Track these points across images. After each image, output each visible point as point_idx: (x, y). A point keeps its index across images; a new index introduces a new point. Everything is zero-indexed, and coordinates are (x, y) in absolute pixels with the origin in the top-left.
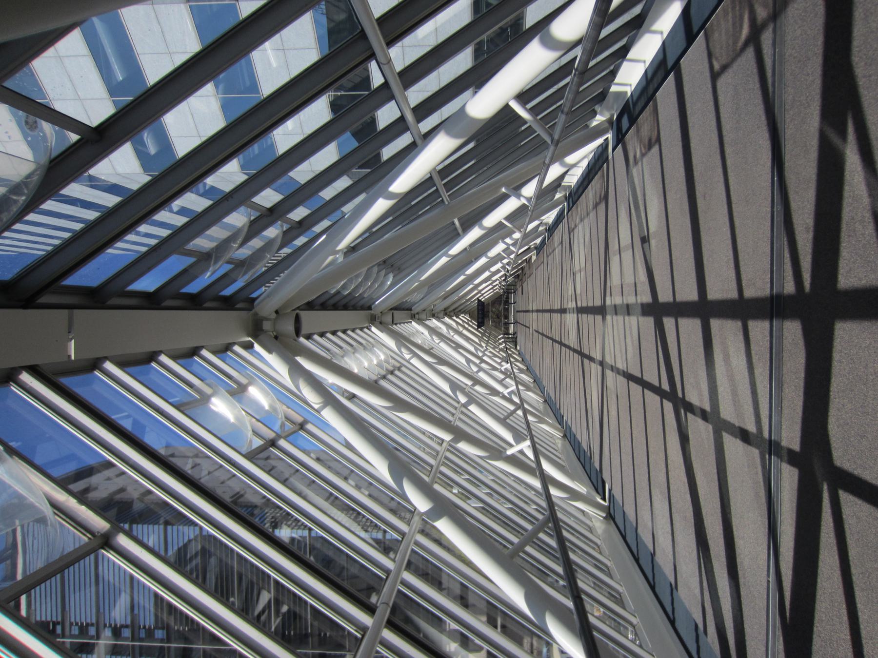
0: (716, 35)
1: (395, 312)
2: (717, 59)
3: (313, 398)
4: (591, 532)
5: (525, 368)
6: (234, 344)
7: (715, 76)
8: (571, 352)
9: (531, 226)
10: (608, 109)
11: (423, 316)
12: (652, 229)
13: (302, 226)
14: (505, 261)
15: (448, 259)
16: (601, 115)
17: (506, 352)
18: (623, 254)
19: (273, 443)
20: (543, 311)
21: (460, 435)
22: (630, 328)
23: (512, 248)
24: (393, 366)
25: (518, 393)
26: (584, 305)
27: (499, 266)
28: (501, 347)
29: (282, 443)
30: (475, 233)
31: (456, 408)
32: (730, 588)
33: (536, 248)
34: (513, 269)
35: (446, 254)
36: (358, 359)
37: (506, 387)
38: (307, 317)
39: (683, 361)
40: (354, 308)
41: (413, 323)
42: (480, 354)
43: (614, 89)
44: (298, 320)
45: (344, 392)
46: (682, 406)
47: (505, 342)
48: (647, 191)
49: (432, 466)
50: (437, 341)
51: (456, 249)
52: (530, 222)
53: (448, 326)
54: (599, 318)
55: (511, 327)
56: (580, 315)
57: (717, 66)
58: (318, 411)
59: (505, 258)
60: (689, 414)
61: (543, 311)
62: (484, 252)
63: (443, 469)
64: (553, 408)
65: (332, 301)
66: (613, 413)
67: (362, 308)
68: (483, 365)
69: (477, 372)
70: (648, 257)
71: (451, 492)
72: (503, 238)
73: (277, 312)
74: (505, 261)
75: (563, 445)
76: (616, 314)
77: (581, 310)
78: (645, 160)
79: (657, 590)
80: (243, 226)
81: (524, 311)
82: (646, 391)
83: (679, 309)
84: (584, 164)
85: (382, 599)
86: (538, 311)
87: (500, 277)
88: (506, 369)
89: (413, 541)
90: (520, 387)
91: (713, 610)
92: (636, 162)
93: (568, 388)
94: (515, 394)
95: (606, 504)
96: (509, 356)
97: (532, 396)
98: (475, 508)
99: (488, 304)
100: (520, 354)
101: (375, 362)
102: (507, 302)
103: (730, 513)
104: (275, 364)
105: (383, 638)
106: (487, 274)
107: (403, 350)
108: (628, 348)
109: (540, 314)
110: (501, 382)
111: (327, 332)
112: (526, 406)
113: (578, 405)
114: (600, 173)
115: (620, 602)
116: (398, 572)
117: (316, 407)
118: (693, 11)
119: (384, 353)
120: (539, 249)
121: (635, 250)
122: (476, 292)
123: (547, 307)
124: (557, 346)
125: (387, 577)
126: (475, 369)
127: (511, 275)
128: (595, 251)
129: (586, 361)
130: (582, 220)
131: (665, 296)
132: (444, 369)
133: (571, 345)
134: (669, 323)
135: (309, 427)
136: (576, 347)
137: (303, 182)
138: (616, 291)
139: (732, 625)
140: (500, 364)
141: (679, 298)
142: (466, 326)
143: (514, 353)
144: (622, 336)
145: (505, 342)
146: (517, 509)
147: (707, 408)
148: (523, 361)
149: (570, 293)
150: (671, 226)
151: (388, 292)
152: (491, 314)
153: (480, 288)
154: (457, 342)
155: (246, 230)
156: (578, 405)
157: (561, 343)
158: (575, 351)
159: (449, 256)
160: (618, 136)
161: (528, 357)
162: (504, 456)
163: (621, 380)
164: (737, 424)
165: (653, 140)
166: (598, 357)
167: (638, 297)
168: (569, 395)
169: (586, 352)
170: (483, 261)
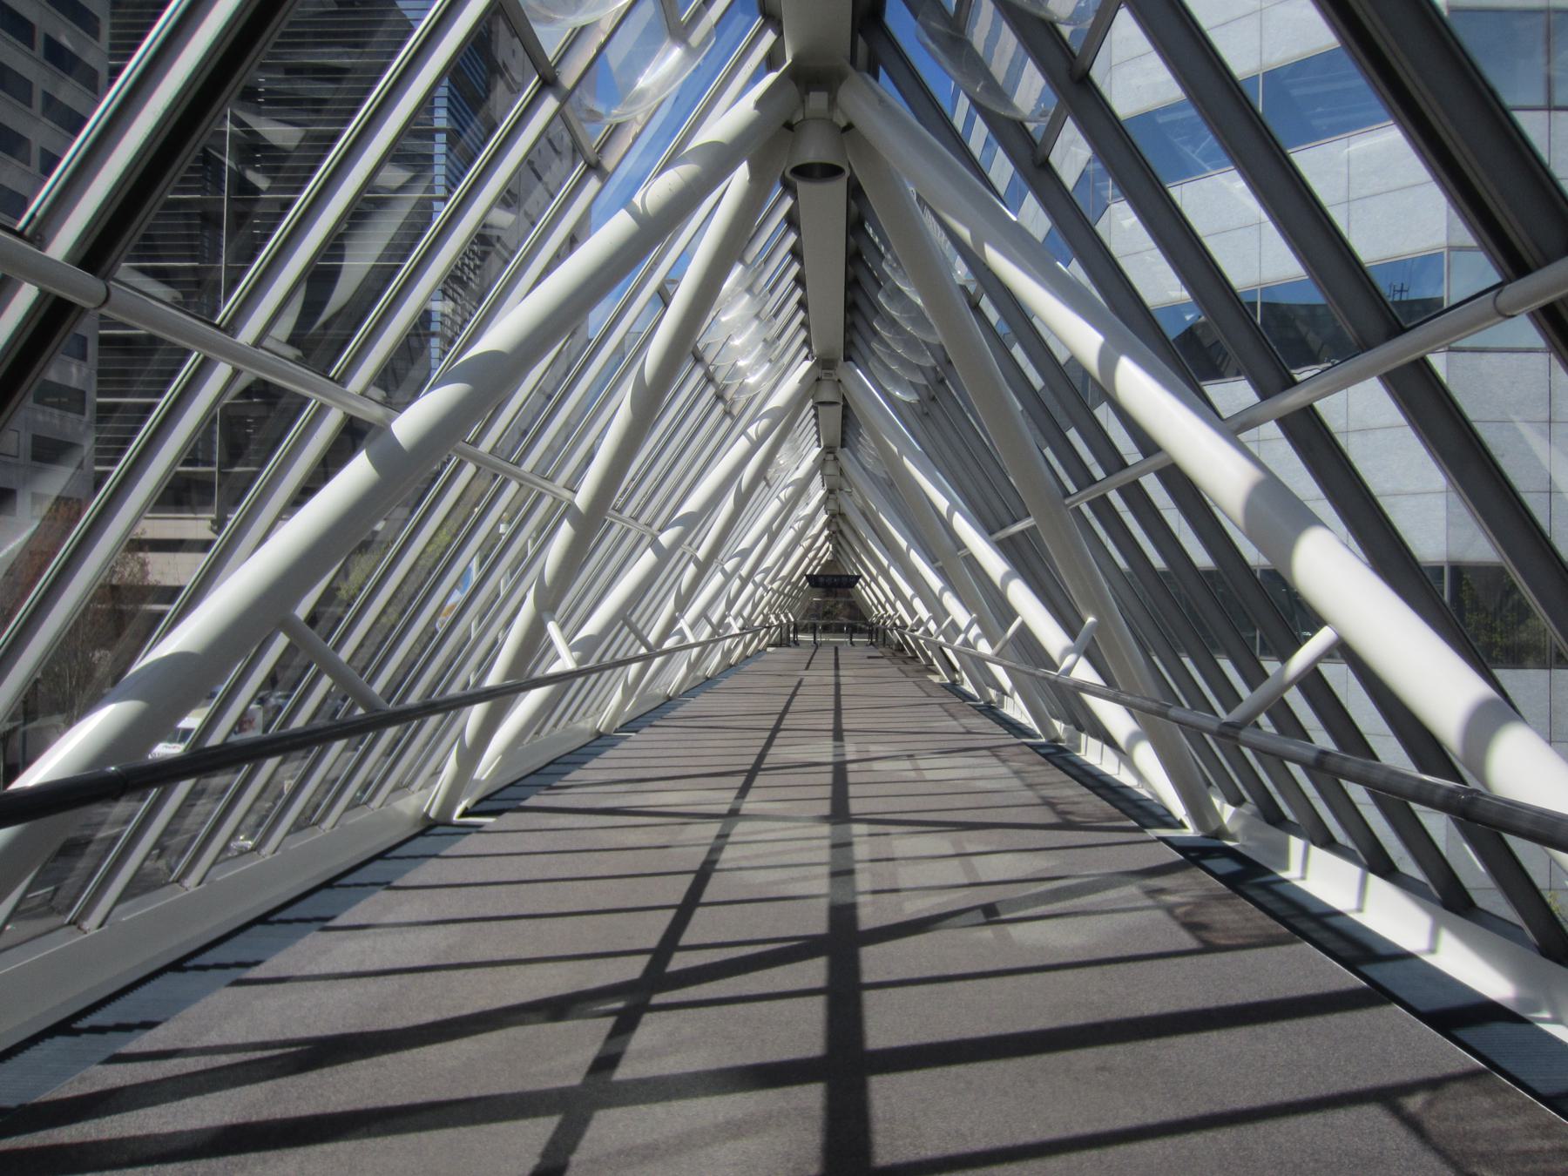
0: (1486, 1103)
1: (839, 408)
2: (1430, 1104)
3: (657, 190)
4: (394, 790)
5: (733, 661)
6: (780, 34)
7: (1388, 1097)
8: (758, 750)
9: (999, 672)
10: (1246, 829)
11: (830, 469)
12: (1016, 931)
13: (1036, 169)
14: (932, 626)
15: (944, 511)
16: (1235, 816)
17: (762, 626)
18: (956, 861)
19: (549, 83)
20: (838, 696)
21: (590, 524)
22: (805, 879)
23: (961, 637)
24: (733, 402)
25: (684, 647)
26: (851, 778)
27: (923, 613)
28: (772, 618)
29: (550, 105)
30: (995, 564)
31: (650, 525)
32: (194, 1133)
33: (954, 683)
34: (916, 640)
35: (953, 507)
36: (746, 325)
37: (692, 627)
38: (828, 199)
39: (732, 1007)
40: (850, 327)
41: (817, 451)
42: (758, 578)
43: (1296, 844)
44: (830, 172)
45: (671, 282)
46: (631, 1005)
47: (781, 625)
48: (1093, 919)
49: (518, 463)
50: (782, 495)
51: (963, 527)
52: (1008, 669)
53: (811, 519)
54: (825, 808)
55: (808, 638)
56: (830, 768)
57: (1414, 1103)
58: (626, 203)
59: (939, 624)
60: (609, 1022)
61: (838, 696)
62: (961, 586)
63: (513, 487)
64: (654, 713)
65: (862, 302)
66: (633, 838)
67: (849, 345)
68: (736, 583)
69: (724, 572)
70: (956, 920)
71: (499, 520)
72: (979, 621)
73: (849, 127)
74: (932, 626)
75: (583, 732)
76: (834, 846)
77: (840, 771)
78: (1160, 915)
79: (259, 928)
80: (1047, 11)
81: (837, 660)
82: (671, 913)
83: (844, 998)
84: (1126, 778)
85: (141, 298)
86: (838, 685)
87: (900, 618)
88: (729, 625)
89: (326, 401)
90: (696, 651)
91: (158, 1082)
92: (1152, 893)
93: (689, 744)
94: (681, 641)
95: (455, 818)
96: (756, 632)
97: (677, 674)
98: (467, 569)
99: (849, 596)
100: (758, 652)
101: (741, 363)
102: (853, 630)
103: (369, 1135)
104: (731, 116)
105: (215, 364)
106: (908, 591)
107: (765, 423)
108: (762, 873)
109: (831, 690)
110: (704, 615)
111: (804, 290)
112: (658, 661)
113: (653, 762)
114: (1115, 812)
115: (140, 886)
116: (233, 354)
117: (637, 199)
118: (1500, 1028)
119: (759, 384)
120: (954, 688)
121: (966, 891)
122: (874, 572)
123: (845, 702)
124: (770, 722)
125: (217, 327)
126: (729, 566)
127: (902, 636)
128: (959, 802)
129: (739, 781)
130: (1017, 773)
131: (875, 961)
132: (728, 504)
133: (772, 750)
134: (814, 971)
135: (593, 184)
136: (769, 760)
137: (1100, 228)
138: (882, 847)
139: (105, 1136)
140: (740, 613)
141: (870, 998)
142: (811, 555)
143: (760, 641)
144: (786, 859)
145: (781, 625)
146: (431, 641)
147: (622, 1073)
148: (745, 658)
149: (873, 748)
150: (1025, 978)
151: (879, 394)
152: (831, 600)
153: (881, 579)
154: (780, 537)
155: (1042, 14)
156: (653, 762)
157: (776, 730)
158: (761, 756)
159: (1107, 362)
160: (1194, 849)
161: (753, 666)
162: (545, 615)
163: (700, 855)
164: (574, 1159)
165: (1206, 935)
166: (748, 806)
167: (868, 898)
168: (676, 744)
169: (760, 780)
170: (936, 583)
